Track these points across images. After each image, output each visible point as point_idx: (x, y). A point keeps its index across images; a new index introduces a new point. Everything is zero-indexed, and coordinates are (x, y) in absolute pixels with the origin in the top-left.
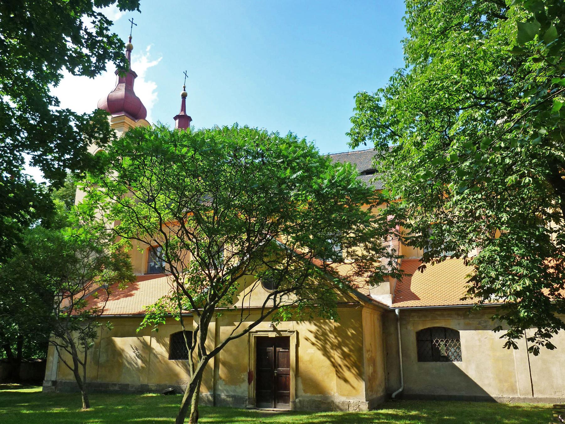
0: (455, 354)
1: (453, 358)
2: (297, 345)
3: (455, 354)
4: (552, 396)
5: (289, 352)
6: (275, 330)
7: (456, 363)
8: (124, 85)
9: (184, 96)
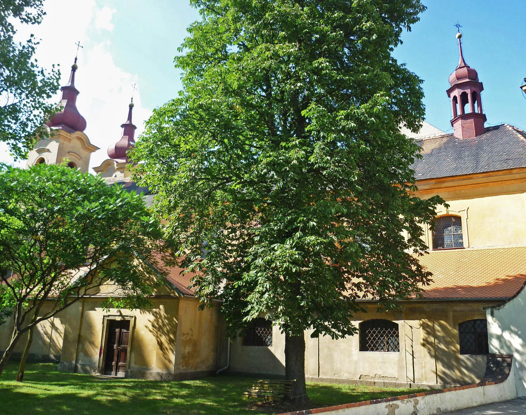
4: (332, 378)
6: (121, 315)
8: (66, 101)
9: (131, 107)
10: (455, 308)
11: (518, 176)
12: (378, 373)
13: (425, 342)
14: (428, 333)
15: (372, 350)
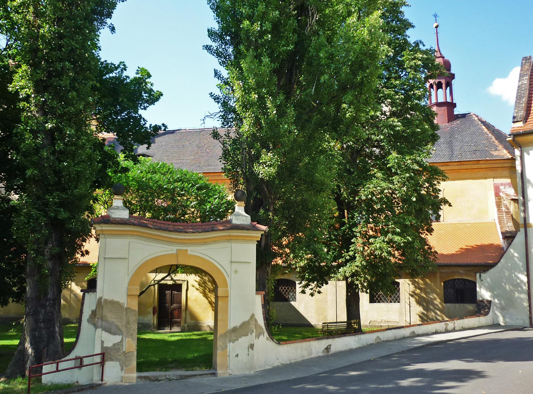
0: (293, 297)
1: (291, 299)
2: (187, 290)
3: (293, 297)
5: (181, 294)
7: (292, 303)
10: (442, 271)
11: (483, 166)
12: (384, 319)
13: (413, 294)
14: (416, 287)
15: (379, 302)
